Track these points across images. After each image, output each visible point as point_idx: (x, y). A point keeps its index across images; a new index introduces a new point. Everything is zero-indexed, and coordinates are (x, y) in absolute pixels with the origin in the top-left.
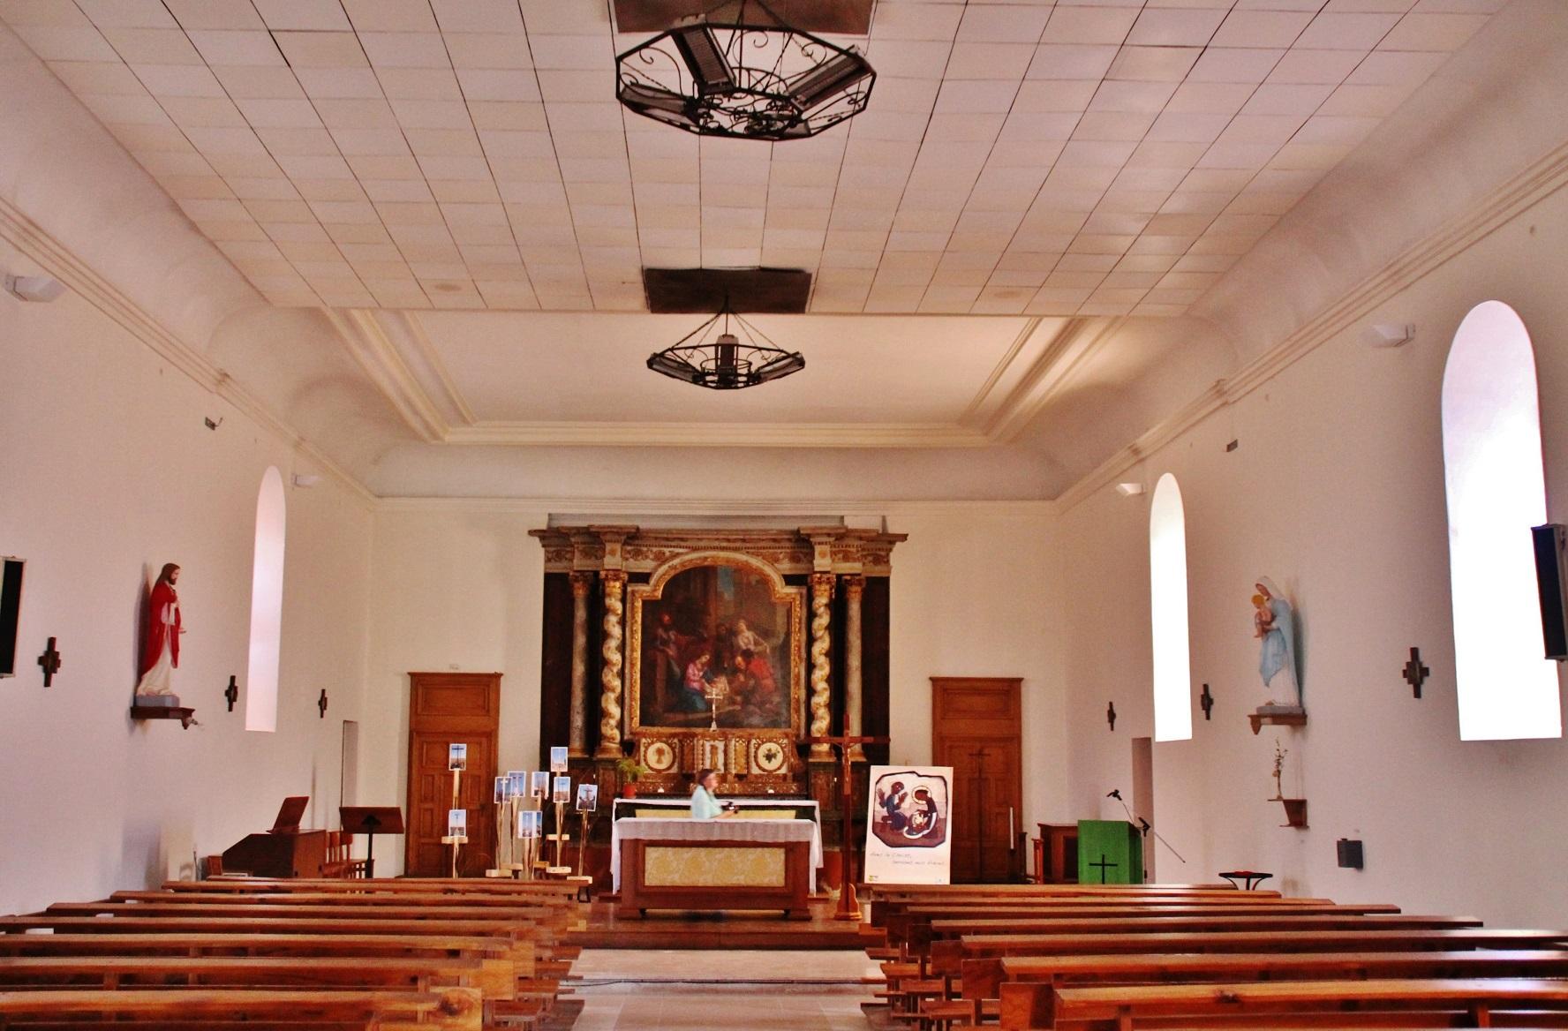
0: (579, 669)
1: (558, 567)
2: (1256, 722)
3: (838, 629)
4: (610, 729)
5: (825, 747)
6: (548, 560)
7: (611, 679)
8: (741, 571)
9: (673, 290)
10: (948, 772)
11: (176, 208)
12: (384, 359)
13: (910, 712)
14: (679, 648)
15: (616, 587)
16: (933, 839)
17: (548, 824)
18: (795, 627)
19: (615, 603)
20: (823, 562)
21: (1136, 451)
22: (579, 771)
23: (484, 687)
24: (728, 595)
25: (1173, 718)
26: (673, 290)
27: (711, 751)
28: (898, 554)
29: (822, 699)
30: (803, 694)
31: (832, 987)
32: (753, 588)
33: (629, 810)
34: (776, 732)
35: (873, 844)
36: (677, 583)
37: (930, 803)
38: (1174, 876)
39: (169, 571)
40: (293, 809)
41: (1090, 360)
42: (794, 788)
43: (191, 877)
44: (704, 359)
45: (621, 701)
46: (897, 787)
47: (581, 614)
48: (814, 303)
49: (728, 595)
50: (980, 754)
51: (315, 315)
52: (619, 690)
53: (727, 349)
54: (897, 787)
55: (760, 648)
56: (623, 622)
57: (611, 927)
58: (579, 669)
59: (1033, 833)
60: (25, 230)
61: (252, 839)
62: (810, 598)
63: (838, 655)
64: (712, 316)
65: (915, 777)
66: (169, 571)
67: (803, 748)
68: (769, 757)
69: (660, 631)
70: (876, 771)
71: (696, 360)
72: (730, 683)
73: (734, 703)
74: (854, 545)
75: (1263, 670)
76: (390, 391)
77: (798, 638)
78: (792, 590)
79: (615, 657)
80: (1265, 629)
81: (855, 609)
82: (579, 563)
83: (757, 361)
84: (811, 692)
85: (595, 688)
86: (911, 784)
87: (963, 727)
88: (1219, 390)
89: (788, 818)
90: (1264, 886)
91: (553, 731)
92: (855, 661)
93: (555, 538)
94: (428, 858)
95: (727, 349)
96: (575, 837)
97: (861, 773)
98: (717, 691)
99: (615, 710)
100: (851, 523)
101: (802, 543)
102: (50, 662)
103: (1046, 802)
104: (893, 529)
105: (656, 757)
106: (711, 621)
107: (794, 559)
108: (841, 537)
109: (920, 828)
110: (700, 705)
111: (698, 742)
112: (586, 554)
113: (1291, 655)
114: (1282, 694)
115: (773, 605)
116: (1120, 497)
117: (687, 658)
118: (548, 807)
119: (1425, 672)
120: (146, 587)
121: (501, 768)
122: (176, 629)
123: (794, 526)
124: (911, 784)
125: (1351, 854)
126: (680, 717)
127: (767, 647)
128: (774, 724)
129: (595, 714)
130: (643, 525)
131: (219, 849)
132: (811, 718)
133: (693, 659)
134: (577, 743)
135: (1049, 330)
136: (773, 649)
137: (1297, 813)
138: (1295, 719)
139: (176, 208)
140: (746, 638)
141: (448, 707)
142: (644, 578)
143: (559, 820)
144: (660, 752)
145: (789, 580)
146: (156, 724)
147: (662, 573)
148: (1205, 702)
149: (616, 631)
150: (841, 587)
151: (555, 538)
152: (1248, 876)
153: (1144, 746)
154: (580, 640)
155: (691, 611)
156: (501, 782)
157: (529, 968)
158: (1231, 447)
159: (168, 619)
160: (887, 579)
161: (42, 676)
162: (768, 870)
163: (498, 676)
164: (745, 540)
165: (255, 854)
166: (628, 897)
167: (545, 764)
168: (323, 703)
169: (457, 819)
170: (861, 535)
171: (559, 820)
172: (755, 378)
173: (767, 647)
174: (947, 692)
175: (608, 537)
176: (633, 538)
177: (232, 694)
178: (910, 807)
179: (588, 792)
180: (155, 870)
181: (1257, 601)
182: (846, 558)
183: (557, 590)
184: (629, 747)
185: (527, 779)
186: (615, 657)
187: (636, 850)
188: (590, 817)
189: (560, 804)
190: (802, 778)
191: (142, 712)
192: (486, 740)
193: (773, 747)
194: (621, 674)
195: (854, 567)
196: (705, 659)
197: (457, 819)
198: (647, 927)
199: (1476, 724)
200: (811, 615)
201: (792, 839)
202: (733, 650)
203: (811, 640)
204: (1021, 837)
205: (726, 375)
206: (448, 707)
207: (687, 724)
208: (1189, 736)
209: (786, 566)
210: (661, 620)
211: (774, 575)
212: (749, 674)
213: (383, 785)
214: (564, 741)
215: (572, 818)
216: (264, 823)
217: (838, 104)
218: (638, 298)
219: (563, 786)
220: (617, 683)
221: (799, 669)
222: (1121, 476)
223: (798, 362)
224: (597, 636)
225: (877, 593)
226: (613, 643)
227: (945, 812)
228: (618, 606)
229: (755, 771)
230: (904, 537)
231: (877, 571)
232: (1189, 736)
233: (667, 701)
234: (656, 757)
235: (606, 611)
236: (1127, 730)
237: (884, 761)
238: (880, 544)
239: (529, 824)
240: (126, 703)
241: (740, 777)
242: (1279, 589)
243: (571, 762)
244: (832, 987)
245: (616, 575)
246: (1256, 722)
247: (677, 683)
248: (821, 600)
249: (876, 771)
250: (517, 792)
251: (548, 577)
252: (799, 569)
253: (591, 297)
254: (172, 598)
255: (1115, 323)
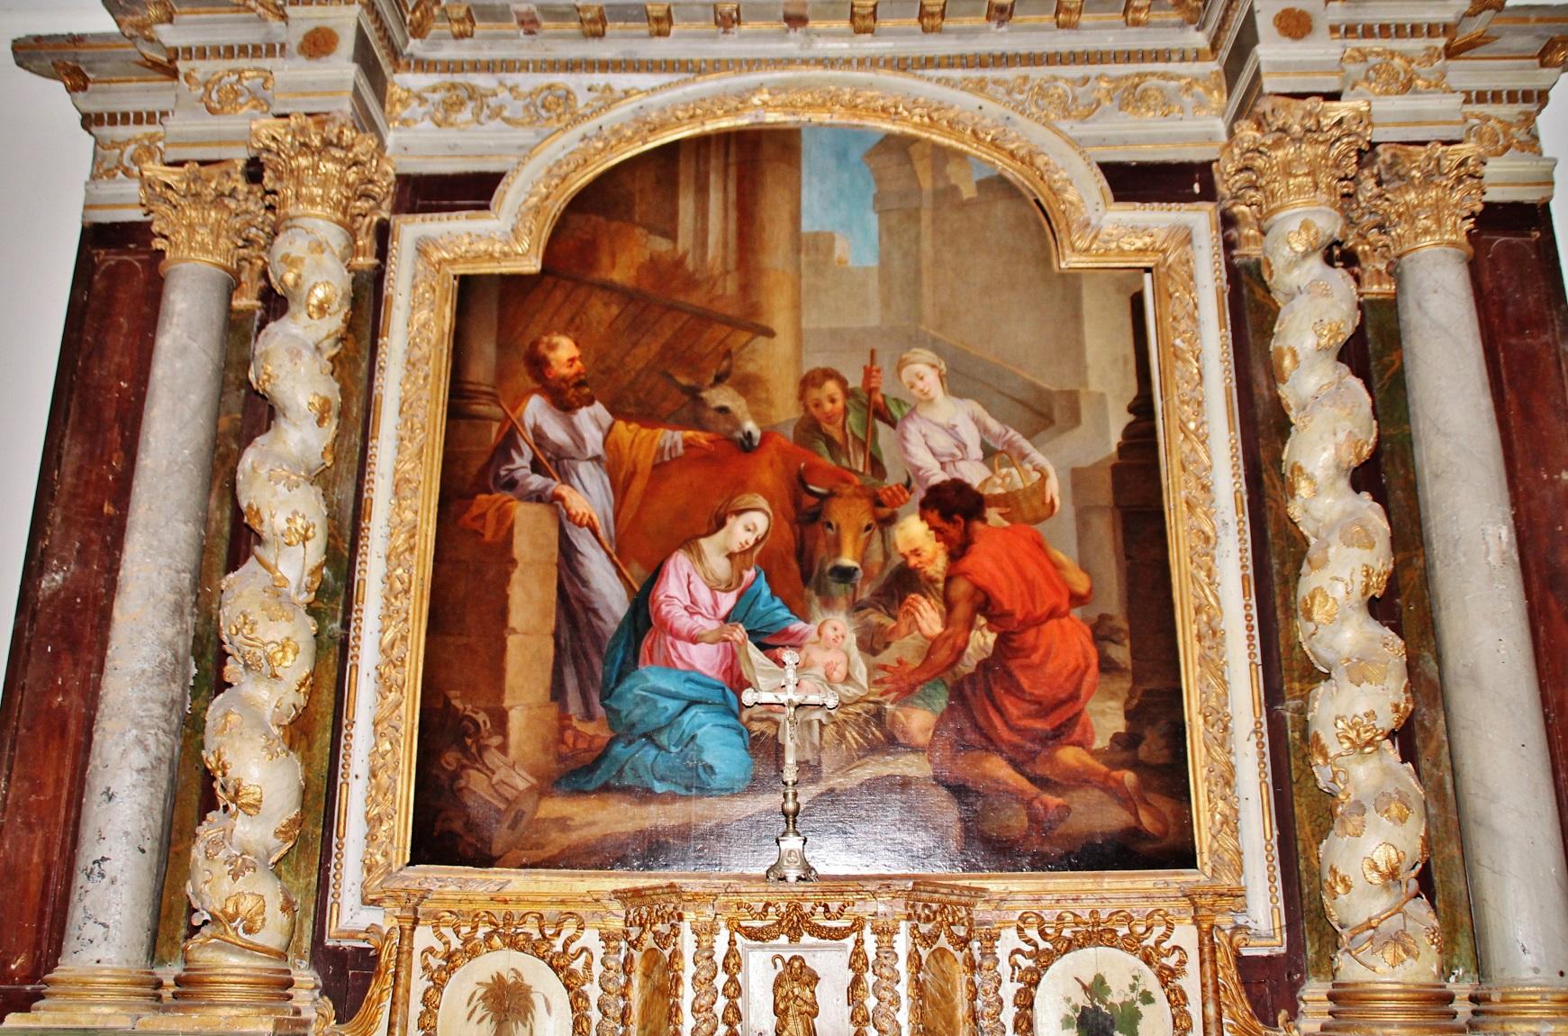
14: (620, 488)
49: (857, 243)
52: (296, 667)
55: (1016, 478)
69: (535, 410)
72: (871, 643)
73: (891, 742)
136: (1078, 479)
175: (850, 590)
210: (538, 364)
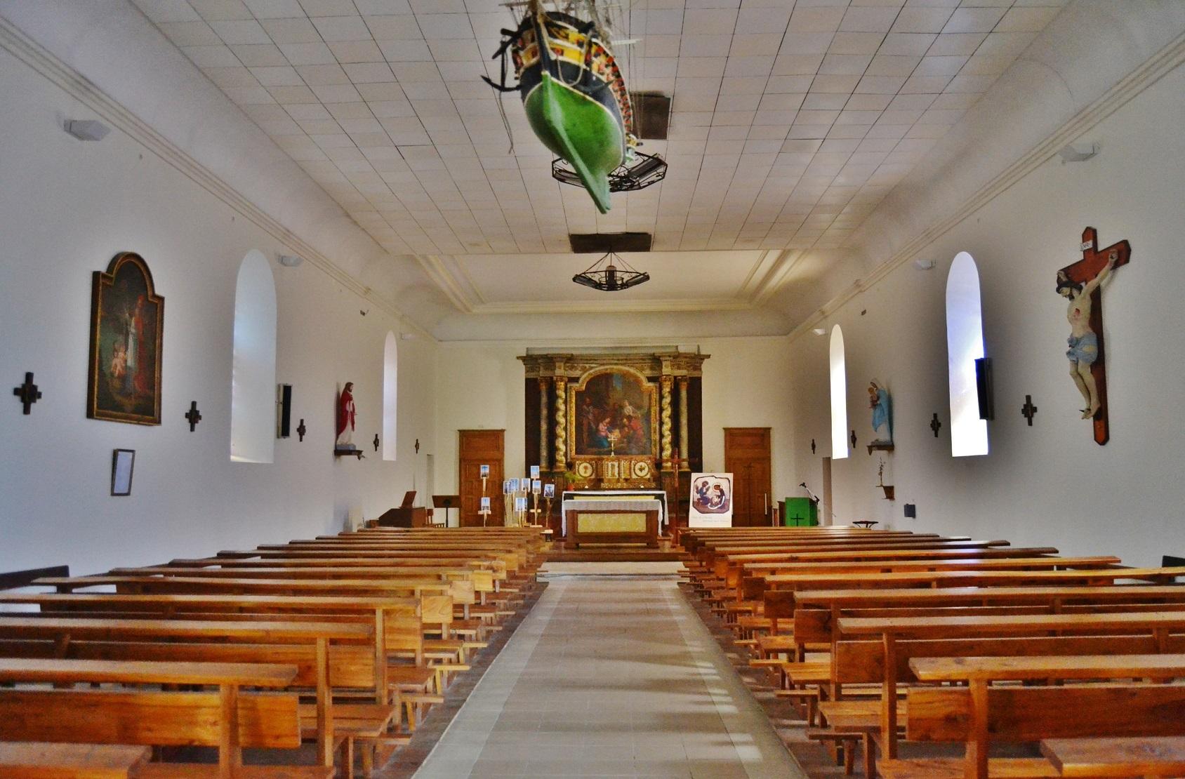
0: (544, 427)
1: (532, 375)
2: (870, 449)
3: (675, 404)
4: (560, 457)
5: (669, 464)
6: (527, 372)
7: (560, 431)
8: (624, 375)
9: (583, 243)
10: (730, 476)
11: (348, 216)
12: (443, 276)
13: (713, 446)
15: (562, 385)
16: (723, 509)
17: (530, 504)
18: (653, 403)
19: (561, 393)
20: (667, 370)
21: (823, 313)
22: (545, 478)
23: (495, 438)
24: (619, 388)
25: (840, 448)
26: (583, 243)
27: (612, 468)
28: (705, 365)
29: (667, 440)
30: (657, 437)
31: (666, 577)
32: (631, 384)
33: (571, 497)
34: (644, 457)
35: (693, 512)
36: (590, 383)
37: (722, 491)
38: (839, 527)
39: (349, 386)
40: (410, 497)
41: (796, 268)
42: (654, 485)
43: (362, 527)
44: (600, 277)
45: (565, 442)
46: (705, 484)
47: (544, 399)
48: (655, 247)
49: (619, 388)
50: (750, 467)
51: (411, 259)
53: (611, 272)
54: (705, 484)
56: (565, 402)
57: (564, 551)
58: (544, 427)
59: (776, 506)
60: (653, 601)
61: (392, 511)
62: (661, 388)
63: (675, 418)
64: (604, 254)
65: (715, 478)
66: (349, 386)
67: (658, 465)
68: (641, 470)
70: (694, 476)
71: (596, 278)
74: (683, 361)
75: (874, 424)
76: (445, 289)
77: (655, 409)
78: (651, 384)
79: (562, 420)
80: (874, 404)
81: (684, 394)
82: (542, 373)
83: (626, 277)
84: (662, 436)
85: (552, 436)
86: (712, 482)
87: (738, 453)
88: (857, 284)
89: (652, 499)
90: (875, 528)
91: (532, 458)
92: (684, 420)
93: (530, 360)
94: (471, 519)
95: (611, 272)
96: (544, 511)
97: (685, 478)
98: (614, 436)
99: (562, 447)
100: (682, 350)
101: (656, 361)
102: (302, 430)
103: (783, 488)
104: (703, 353)
105: (584, 470)
106: (611, 402)
107: (652, 368)
108: (676, 357)
109: (717, 504)
110: (606, 444)
111: (605, 462)
112: (546, 369)
113: (887, 417)
114: (883, 436)
115: (642, 393)
116: (815, 335)
117: (598, 421)
118: (530, 496)
119: (939, 425)
120: (338, 394)
121: (506, 476)
122: (353, 413)
123: (652, 351)
124: (712, 482)
125: (910, 511)
126: (595, 450)
127: (639, 414)
128: (643, 453)
129: (553, 449)
130: (574, 352)
131: (376, 516)
132: (662, 449)
133: (602, 420)
134: (544, 464)
135: (773, 256)
137: (889, 492)
138: (889, 447)
139: (348, 216)
140: (629, 410)
141: (478, 447)
142: (576, 380)
143: (536, 502)
144: (586, 468)
145: (650, 379)
146: (345, 458)
147: (585, 377)
148: (853, 439)
149: (562, 407)
150: (676, 383)
151: (530, 360)
152: (867, 523)
153: (828, 461)
154: (544, 412)
155: (599, 396)
156: (507, 484)
157: (523, 560)
158: (864, 313)
159: (349, 408)
160: (700, 379)
161: (188, 425)
162: (638, 524)
163: (503, 431)
164: (627, 360)
165: (391, 518)
166: (570, 539)
167: (528, 474)
168: (417, 446)
169: (485, 502)
170: (686, 356)
171: (536, 502)
172: (625, 285)
173: (639, 414)
174: (733, 436)
176: (570, 360)
177: (376, 443)
178: (712, 494)
179: (549, 488)
180: (347, 524)
181: (871, 390)
182: (679, 368)
183: (532, 387)
184: (570, 466)
185: (519, 483)
186: (562, 420)
187: (573, 515)
188: (551, 500)
189: (536, 494)
190: (658, 480)
191: (339, 452)
192: (498, 463)
193: (643, 464)
194: (565, 429)
195: (683, 372)
196: (608, 420)
197: (485, 502)
198: (580, 551)
199: (959, 450)
200: (661, 397)
201: (649, 508)
202: (622, 416)
203: (661, 410)
204: (770, 508)
205: (611, 283)
206: (478, 447)
207: (599, 453)
208: (846, 456)
209: (648, 372)
211: (642, 377)
212: (630, 427)
213: (450, 488)
214: (537, 463)
215: (542, 502)
216: (397, 504)
217: (652, 176)
218: (568, 246)
219: (537, 486)
220: (563, 433)
221: (655, 425)
222: (816, 325)
223: (646, 278)
224: (553, 410)
225: (695, 386)
226: (561, 413)
227: (729, 495)
228: (563, 395)
229: (634, 476)
230: (709, 356)
231: (695, 374)
232: (846, 456)
233: (589, 443)
234: (584, 470)
235: (557, 397)
236: (820, 455)
237: (700, 470)
238: (696, 360)
239: (521, 505)
240: (332, 449)
241: (626, 480)
242: (882, 385)
243: (541, 473)
244: (666, 577)
245: (561, 378)
246: (870, 449)
247: (594, 433)
248: (666, 390)
249: (694, 476)
250: (514, 489)
251: (528, 381)
252: (655, 374)
253: (545, 245)
254: (350, 399)
255: (806, 252)
